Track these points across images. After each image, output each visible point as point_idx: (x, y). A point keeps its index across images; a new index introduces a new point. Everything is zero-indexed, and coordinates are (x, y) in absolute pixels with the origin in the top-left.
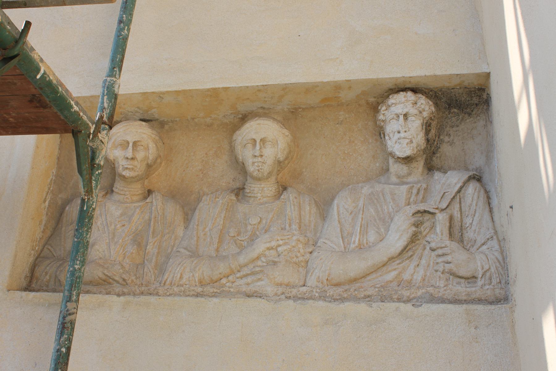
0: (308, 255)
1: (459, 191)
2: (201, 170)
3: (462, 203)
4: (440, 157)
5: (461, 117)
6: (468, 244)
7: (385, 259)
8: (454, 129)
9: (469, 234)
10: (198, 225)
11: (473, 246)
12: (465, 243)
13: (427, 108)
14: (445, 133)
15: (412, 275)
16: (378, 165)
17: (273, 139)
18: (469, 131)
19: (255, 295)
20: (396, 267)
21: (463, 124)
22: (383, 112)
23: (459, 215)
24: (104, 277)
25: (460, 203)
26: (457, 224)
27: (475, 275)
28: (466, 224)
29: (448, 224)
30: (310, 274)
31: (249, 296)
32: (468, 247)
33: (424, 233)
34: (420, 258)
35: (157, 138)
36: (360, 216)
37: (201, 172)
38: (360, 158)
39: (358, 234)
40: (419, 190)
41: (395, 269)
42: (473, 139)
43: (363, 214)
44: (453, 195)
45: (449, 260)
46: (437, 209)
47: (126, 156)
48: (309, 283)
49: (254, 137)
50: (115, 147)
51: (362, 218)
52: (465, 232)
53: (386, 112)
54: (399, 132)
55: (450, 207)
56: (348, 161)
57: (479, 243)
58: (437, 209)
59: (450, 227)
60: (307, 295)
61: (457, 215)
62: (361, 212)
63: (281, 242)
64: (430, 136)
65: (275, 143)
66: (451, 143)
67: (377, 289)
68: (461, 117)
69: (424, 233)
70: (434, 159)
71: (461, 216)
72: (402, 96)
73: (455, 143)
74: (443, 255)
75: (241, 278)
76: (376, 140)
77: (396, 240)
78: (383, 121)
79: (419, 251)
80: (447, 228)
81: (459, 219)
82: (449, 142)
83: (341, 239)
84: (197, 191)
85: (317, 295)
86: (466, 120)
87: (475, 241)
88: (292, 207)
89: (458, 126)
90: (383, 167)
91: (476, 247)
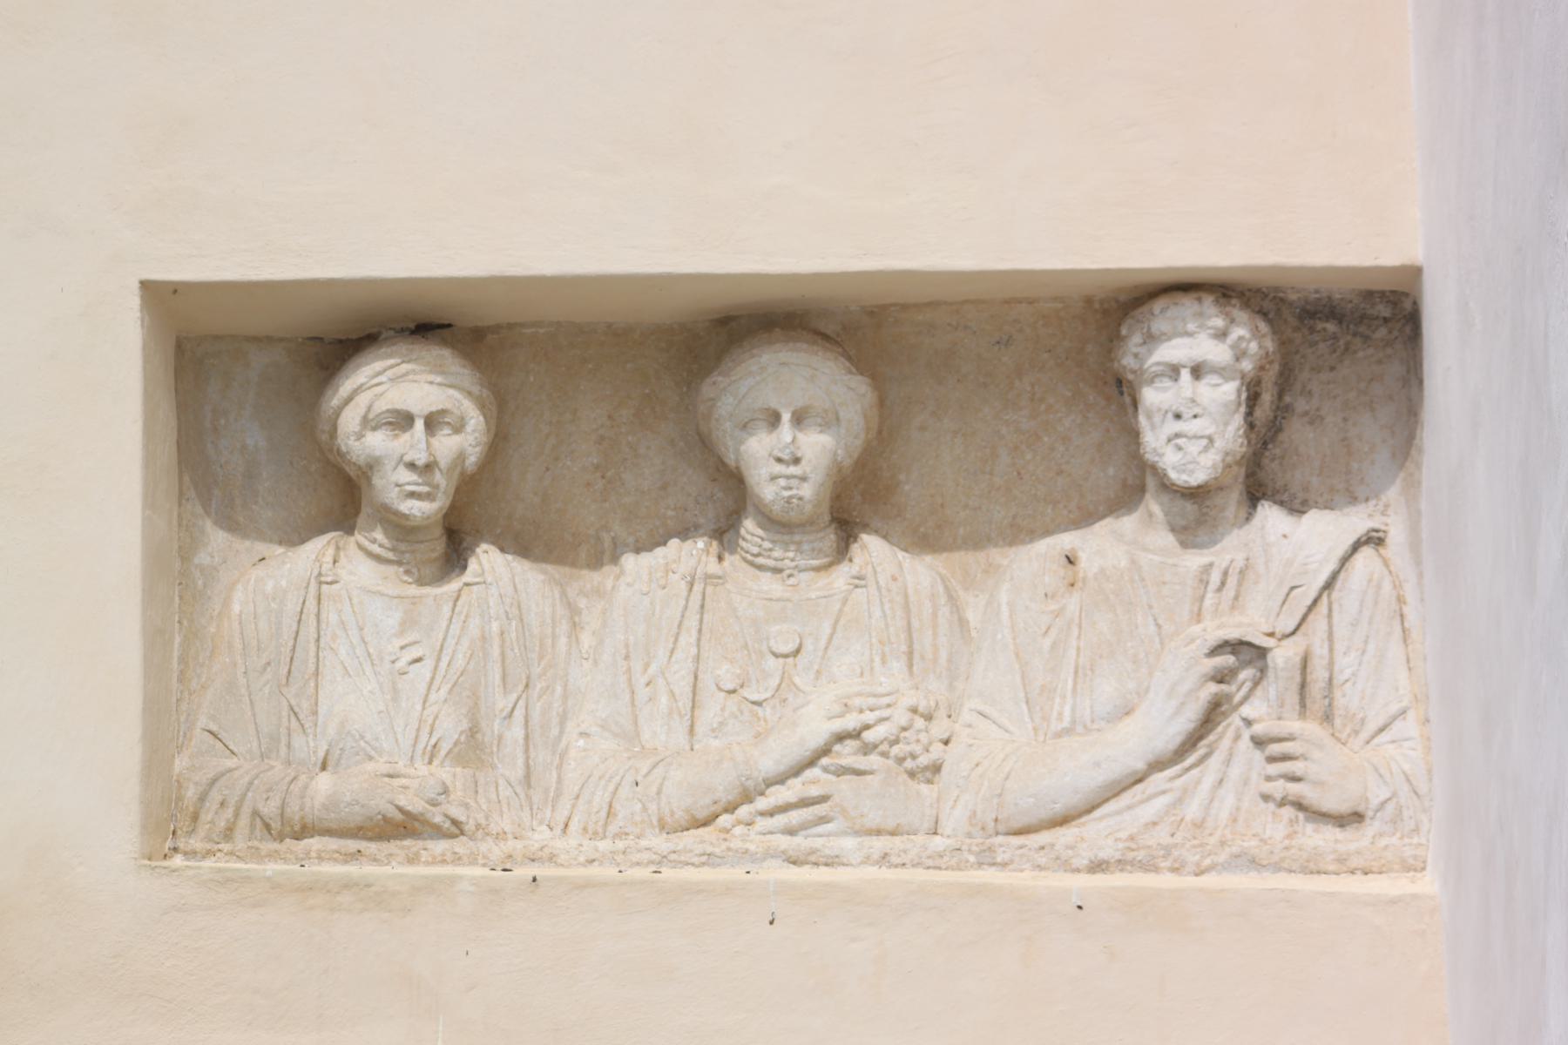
0: (937, 748)
1: (1329, 585)
2: (597, 467)
3: (1335, 614)
4: (1283, 457)
5: (1342, 342)
6: (1345, 725)
7: (1140, 765)
8: (1325, 376)
9: (1347, 699)
10: (627, 657)
11: (1357, 732)
12: (1338, 722)
13: (1253, 347)
14: (1298, 386)
15: (1208, 808)
16: (1111, 471)
17: (826, 411)
18: (1363, 385)
19: (813, 858)
20: (1168, 785)
21: (1347, 363)
22: (1135, 350)
23: (1325, 651)
24: (399, 817)
25: (1330, 616)
26: (1318, 674)
27: (1361, 809)
28: (1342, 671)
29: (1298, 679)
30: (951, 803)
31: (794, 863)
32: (1343, 736)
33: (1237, 699)
34: (1228, 761)
35: (485, 393)
36: (1074, 643)
37: (598, 475)
38: (1062, 449)
39: (1069, 694)
40: (1226, 573)
41: (1164, 792)
42: (1373, 410)
43: (1079, 637)
44: (1313, 595)
45: (1299, 774)
46: (1271, 635)
47: (407, 458)
48: (947, 826)
49: (774, 404)
50: (369, 423)
51: (1078, 649)
52: (1337, 694)
53: (1142, 350)
54: (1178, 416)
55: (1303, 628)
56: (1029, 457)
57: (1371, 727)
58: (1271, 635)
59: (1303, 686)
60: (946, 859)
61: (1320, 651)
62: (1075, 631)
63: (869, 717)
64: (1258, 413)
65: (829, 421)
66: (1315, 419)
67: (1121, 845)
68: (1342, 342)
69: (1237, 699)
70: (1265, 461)
71: (1331, 650)
72: (1187, 306)
73: (1322, 418)
74: (1285, 758)
75: (771, 813)
76: (1108, 399)
77: (1162, 722)
78: (1134, 372)
79: (1226, 743)
80: (1295, 687)
81: (1325, 662)
82: (1306, 413)
83: (1024, 706)
84: (592, 532)
85: (972, 859)
86: (1355, 352)
87: (1363, 720)
88: (887, 606)
89: (1332, 369)
90: (1125, 480)
91: (1364, 735)
